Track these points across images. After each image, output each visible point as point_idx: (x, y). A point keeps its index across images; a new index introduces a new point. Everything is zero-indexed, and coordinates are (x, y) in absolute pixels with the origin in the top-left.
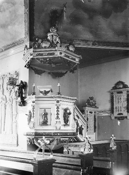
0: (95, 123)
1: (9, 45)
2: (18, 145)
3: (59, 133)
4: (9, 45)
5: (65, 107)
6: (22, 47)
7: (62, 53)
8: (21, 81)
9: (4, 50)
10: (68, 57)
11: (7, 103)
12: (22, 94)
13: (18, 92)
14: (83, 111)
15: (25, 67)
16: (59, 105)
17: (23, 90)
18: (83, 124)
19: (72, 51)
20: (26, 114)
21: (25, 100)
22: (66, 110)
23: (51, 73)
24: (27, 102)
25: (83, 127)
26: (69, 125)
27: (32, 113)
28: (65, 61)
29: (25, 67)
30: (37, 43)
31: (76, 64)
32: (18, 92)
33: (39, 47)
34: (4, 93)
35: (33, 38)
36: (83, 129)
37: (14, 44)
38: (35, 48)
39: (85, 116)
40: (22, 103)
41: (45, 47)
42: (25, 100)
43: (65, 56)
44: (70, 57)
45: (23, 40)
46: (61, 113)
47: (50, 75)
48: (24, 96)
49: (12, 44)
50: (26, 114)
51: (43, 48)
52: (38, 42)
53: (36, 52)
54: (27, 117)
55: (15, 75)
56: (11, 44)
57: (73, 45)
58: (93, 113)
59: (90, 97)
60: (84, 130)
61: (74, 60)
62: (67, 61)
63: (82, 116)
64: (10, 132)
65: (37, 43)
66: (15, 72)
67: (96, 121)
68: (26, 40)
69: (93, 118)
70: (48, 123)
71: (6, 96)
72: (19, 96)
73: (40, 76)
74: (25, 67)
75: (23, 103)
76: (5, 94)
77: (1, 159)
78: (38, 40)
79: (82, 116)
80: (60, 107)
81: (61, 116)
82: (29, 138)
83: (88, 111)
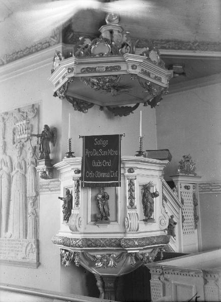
0: (195, 209)
1: (17, 53)
2: (39, 264)
3: (136, 239)
4: (17, 53)
5: (145, 181)
6: (52, 50)
7: (136, 66)
8: (46, 126)
9: (5, 62)
10: (148, 74)
11: (14, 172)
12: (48, 153)
13: (128, 219)
14: (172, 184)
15: (55, 95)
16: (134, 178)
17: (50, 144)
18: (175, 213)
19: (154, 63)
20: (59, 198)
21: (56, 165)
22: (146, 188)
23: (106, 109)
24: (59, 171)
25: (175, 220)
26: (152, 220)
27: (74, 195)
28: (141, 84)
29: (55, 95)
30: (80, 45)
31: (163, 89)
32: (40, 149)
33: (89, 54)
34: (6, 151)
35: (70, 37)
36: (175, 224)
37: (28, 50)
38: (78, 56)
39: (178, 196)
40: (49, 172)
41: (101, 55)
42: (56, 165)
43: (82, 73)
44: (151, 75)
45: (49, 42)
46: (138, 193)
47: (102, 112)
48: (51, 156)
49: (25, 50)
50: (59, 198)
51: (95, 55)
52: (82, 43)
53: (80, 64)
54: (62, 202)
55: (32, 113)
56: (21, 51)
57: (157, 50)
58: (191, 190)
59: (187, 159)
60: (177, 226)
61: (160, 80)
62: (146, 84)
63: (171, 195)
64: (22, 235)
65: (80, 45)
66: (31, 106)
67: (197, 204)
68: (55, 41)
69: (192, 198)
70: (110, 218)
71: (12, 157)
72: (42, 158)
73: (83, 114)
74: (54, 96)
75: (52, 171)
76: (9, 152)
77: (2, 292)
78: (83, 40)
79: (171, 195)
80: (135, 182)
81: (138, 202)
82: (66, 251)
83: (183, 185)
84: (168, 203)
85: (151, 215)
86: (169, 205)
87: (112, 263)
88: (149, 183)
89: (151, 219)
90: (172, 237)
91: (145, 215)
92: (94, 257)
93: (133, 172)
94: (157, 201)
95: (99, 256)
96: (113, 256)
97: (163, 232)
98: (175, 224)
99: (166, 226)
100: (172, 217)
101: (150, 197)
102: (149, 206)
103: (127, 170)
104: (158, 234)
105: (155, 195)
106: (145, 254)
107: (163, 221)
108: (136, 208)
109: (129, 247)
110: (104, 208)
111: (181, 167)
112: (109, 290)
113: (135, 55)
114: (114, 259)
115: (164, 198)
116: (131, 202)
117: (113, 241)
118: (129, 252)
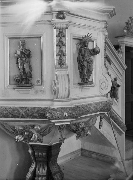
5: (82, 33)
25: (118, 82)
36: (119, 86)
60: (120, 89)
70: (34, 81)
80: (67, 32)
81: (70, 59)
84: (111, 65)
85: (89, 78)
86: (113, 67)
87: (36, 136)
88: (87, 36)
89: (89, 82)
90: (115, 99)
91: (81, 77)
92: (13, 129)
93: (64, 18)
94: (98, 61)
95: (21, 128)
96: (37, 128)
97: (105, 98)
98: (119, 86)
99: (109, 89)
100: (115, 79)
101: (87, 55)
102: (86, 65)
103: (55, 15)
104: (98, 100)
105: (95, 52)
106: (79, 123)
107: (104, 84)
108: (66, 68)
109: (55, 119)
110: (24, 68)
111: (127, 27)
112: (41, 160)
113: (125, 152)
114: (38, 132)
115: (107, 58)
116: (61, 59)
117: (36, 110)
118: (56, 124)
